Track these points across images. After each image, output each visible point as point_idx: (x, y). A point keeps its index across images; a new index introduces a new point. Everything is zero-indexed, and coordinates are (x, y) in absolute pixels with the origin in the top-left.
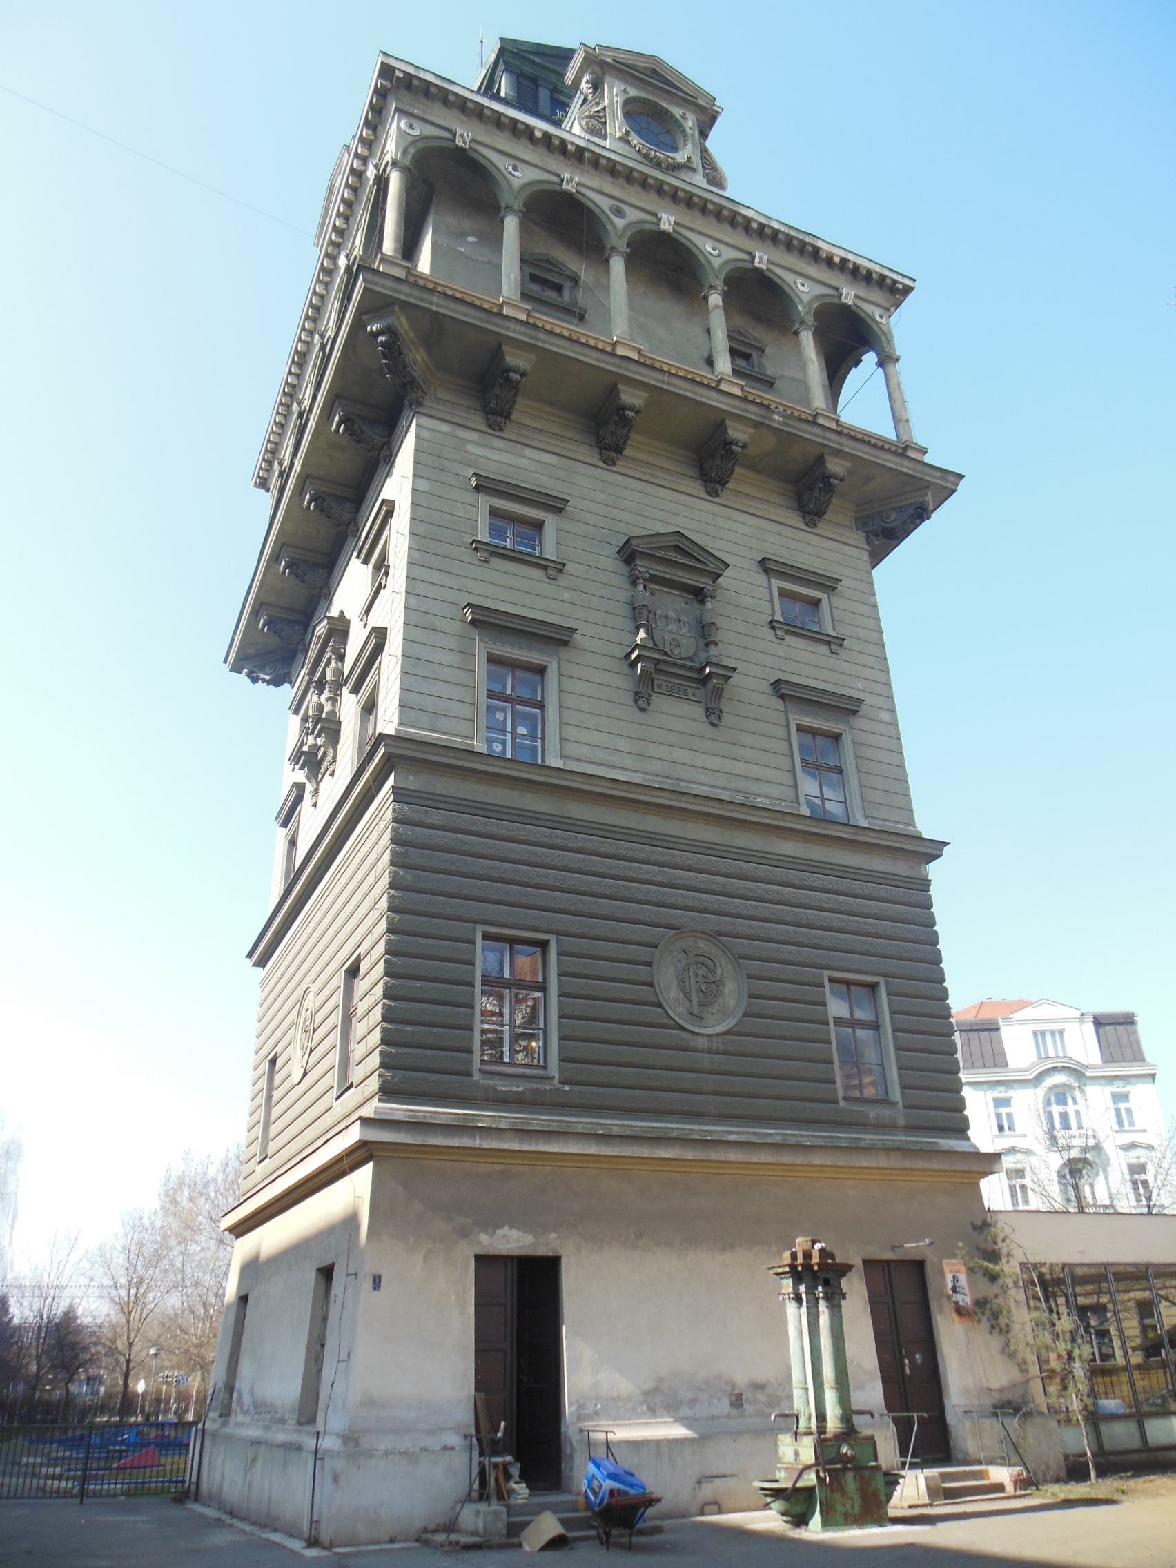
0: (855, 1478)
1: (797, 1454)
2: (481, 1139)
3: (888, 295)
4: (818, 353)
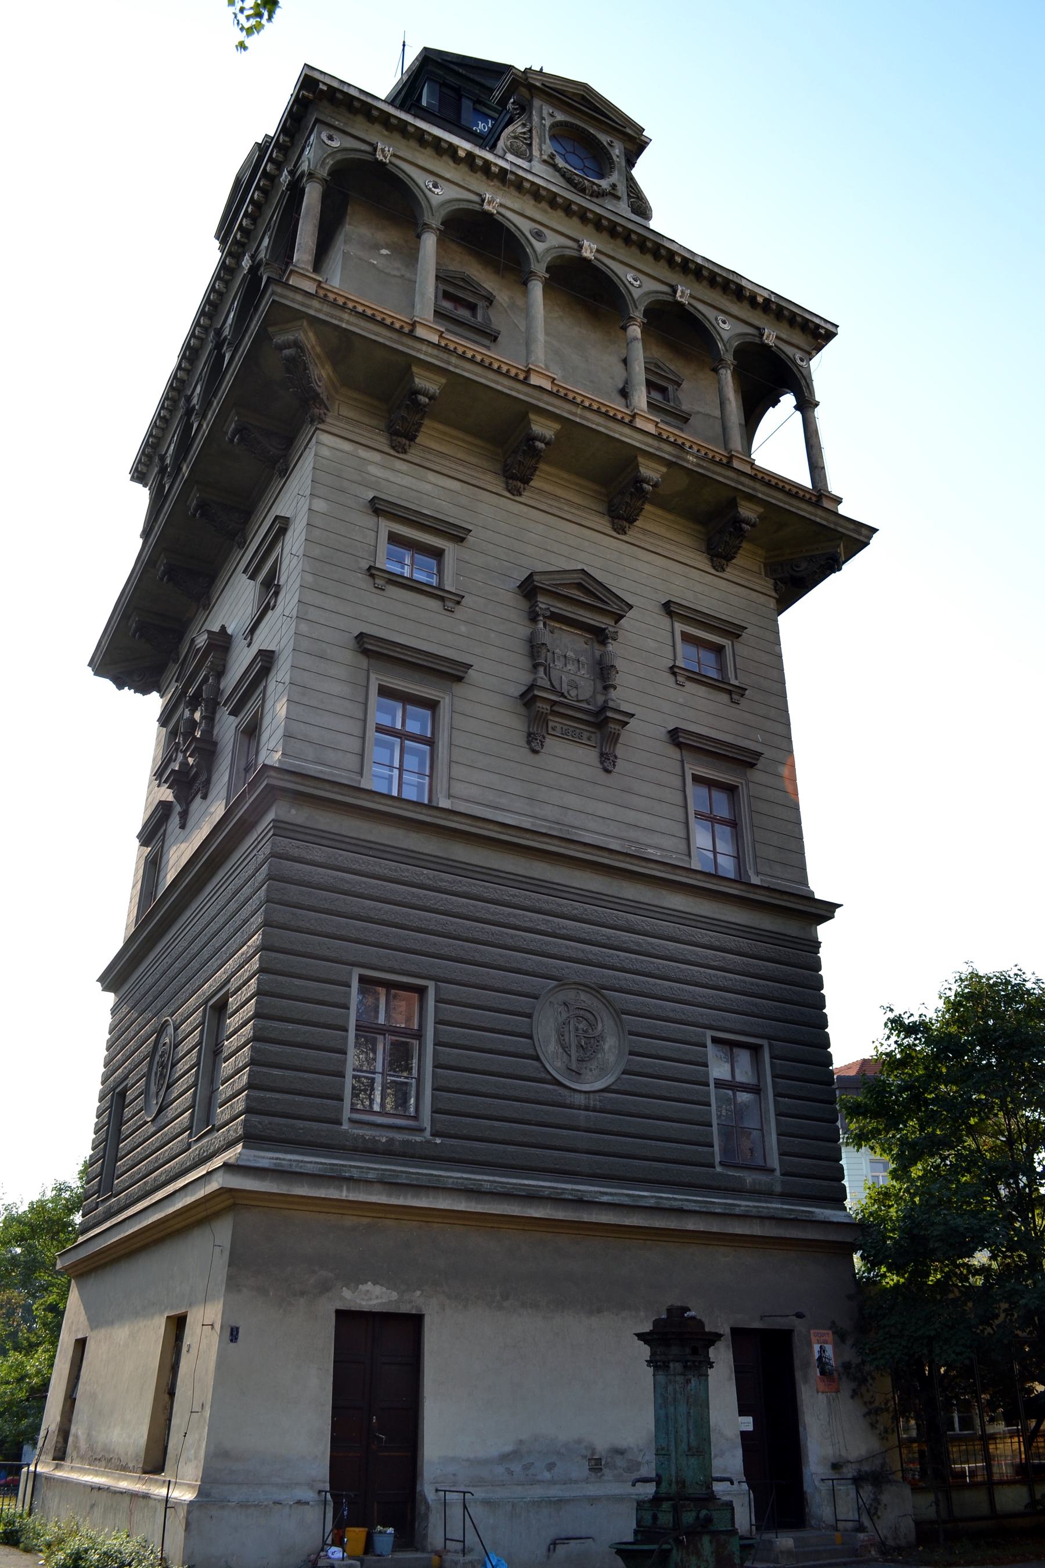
0: (711, 1542)
1: (655, 1518)
2: (348, 1190)
3: (810, 339)
4: (735, 391)
